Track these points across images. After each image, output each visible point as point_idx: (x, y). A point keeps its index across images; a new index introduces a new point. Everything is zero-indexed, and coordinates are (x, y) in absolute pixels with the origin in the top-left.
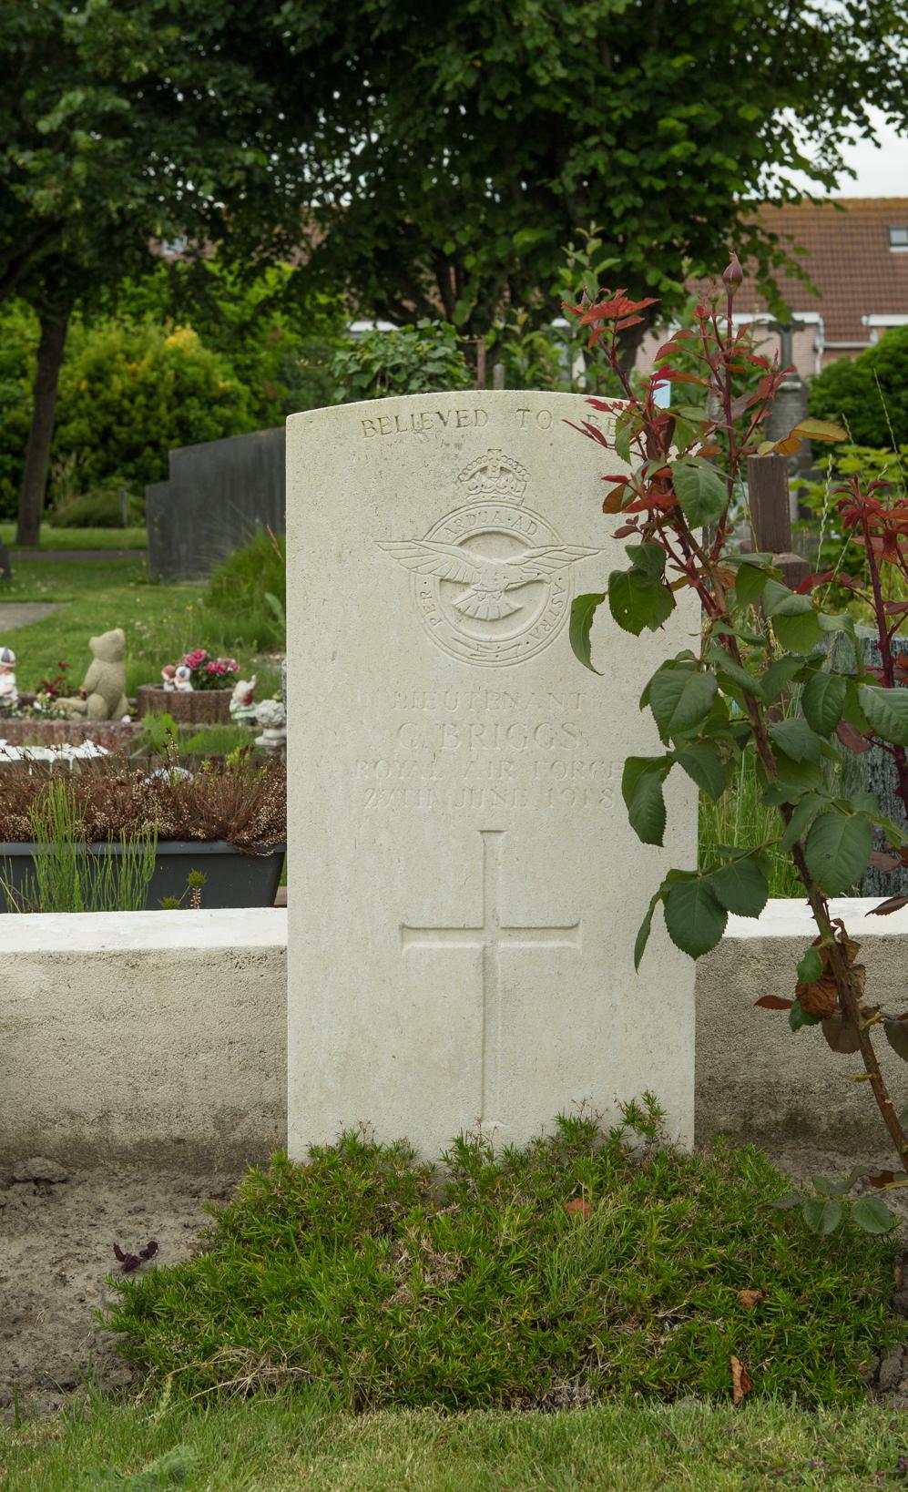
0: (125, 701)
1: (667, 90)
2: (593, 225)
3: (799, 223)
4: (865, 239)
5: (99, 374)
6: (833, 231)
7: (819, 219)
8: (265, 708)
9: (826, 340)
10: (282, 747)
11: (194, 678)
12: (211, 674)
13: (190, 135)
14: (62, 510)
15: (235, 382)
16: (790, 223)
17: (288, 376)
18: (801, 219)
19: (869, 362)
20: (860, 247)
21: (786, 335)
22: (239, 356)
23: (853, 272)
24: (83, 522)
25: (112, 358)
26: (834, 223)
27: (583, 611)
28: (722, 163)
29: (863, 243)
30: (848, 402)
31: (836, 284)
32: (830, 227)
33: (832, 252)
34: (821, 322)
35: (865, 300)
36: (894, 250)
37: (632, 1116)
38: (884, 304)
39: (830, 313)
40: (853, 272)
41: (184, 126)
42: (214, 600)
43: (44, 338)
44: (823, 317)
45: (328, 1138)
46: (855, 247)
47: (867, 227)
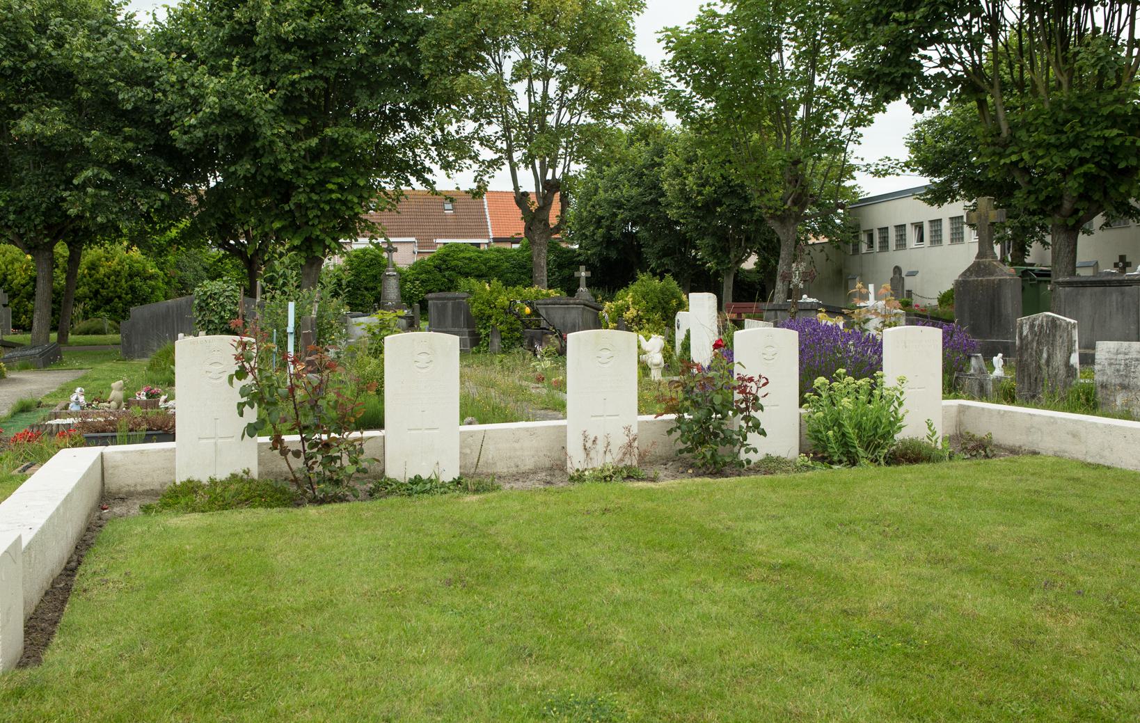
0: (123, 404)
5: (93, 267)
8: (170, 403)
10: (174, 414)
11: (147, 395)
12: (153, 394)
14: (76, 327)
15: (157, 270)
24: (87, 333)
25: (99, 260)
27: (231, 378)
30: (423, 276)
37: (244, 472)
42: (151, 368)
43: (70, 256)
45: (184, 479)
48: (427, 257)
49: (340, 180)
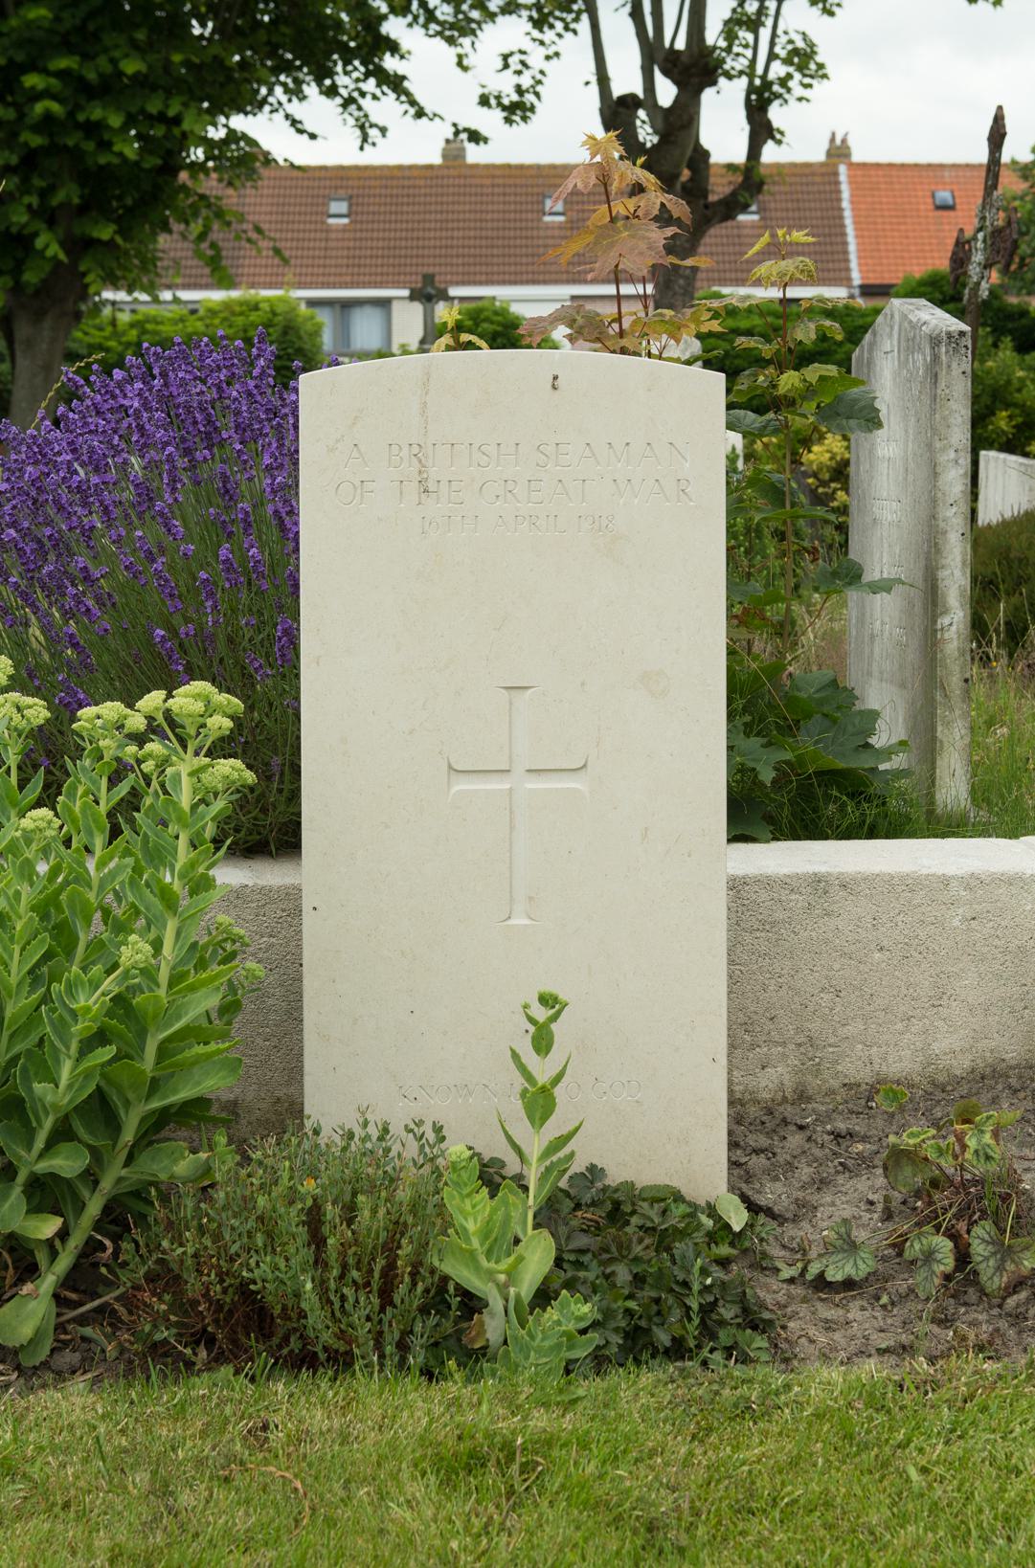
21: (428, 305)
36: (547, 219)
38: (728, 275)
49: (63, 63)
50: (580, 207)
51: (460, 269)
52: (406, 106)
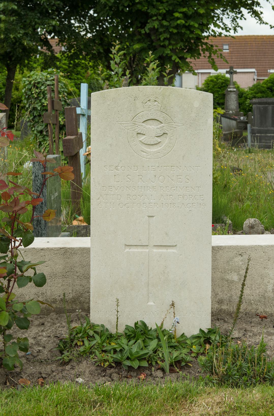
1: (178, 3)
2: (117, 42)
3: (249, 42)
4: (269, 47)
6: (259, 45)
7: (255, 41)
9: (257, 77)
13: (38, 16)
15: (75, 89)
16: (247, 43)
17: (92, 87)
18: (250, 41)
19: (266, 83)
20: (268, 50)
21: (231, 75)
22: (76, 81)
23: (265, 57)
26: (260, 43)
28: (193, 25)
29: (268, 48)
31: (260, 60)
32: (259, 44)
33: (259, 51)
34: (256, 72)
35: (269, 65)
36: (224, 51)
39: (259, 69)
40: (265, 57)
41: (36, 13)
44: (257, 70)
46: (266, 50)
47: (270, 44)
48: (262, 82)
49: (185, 10)
50: (233, 48)
51: (201, 65)
52: (258, 21)
